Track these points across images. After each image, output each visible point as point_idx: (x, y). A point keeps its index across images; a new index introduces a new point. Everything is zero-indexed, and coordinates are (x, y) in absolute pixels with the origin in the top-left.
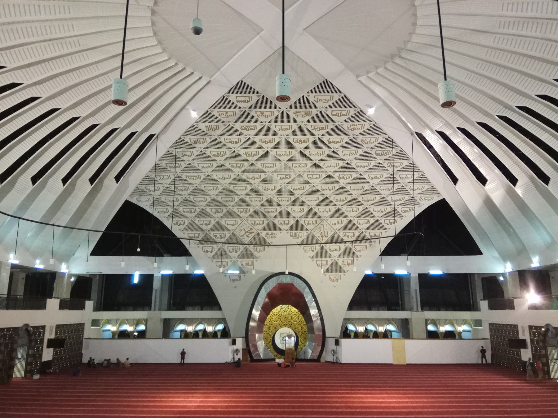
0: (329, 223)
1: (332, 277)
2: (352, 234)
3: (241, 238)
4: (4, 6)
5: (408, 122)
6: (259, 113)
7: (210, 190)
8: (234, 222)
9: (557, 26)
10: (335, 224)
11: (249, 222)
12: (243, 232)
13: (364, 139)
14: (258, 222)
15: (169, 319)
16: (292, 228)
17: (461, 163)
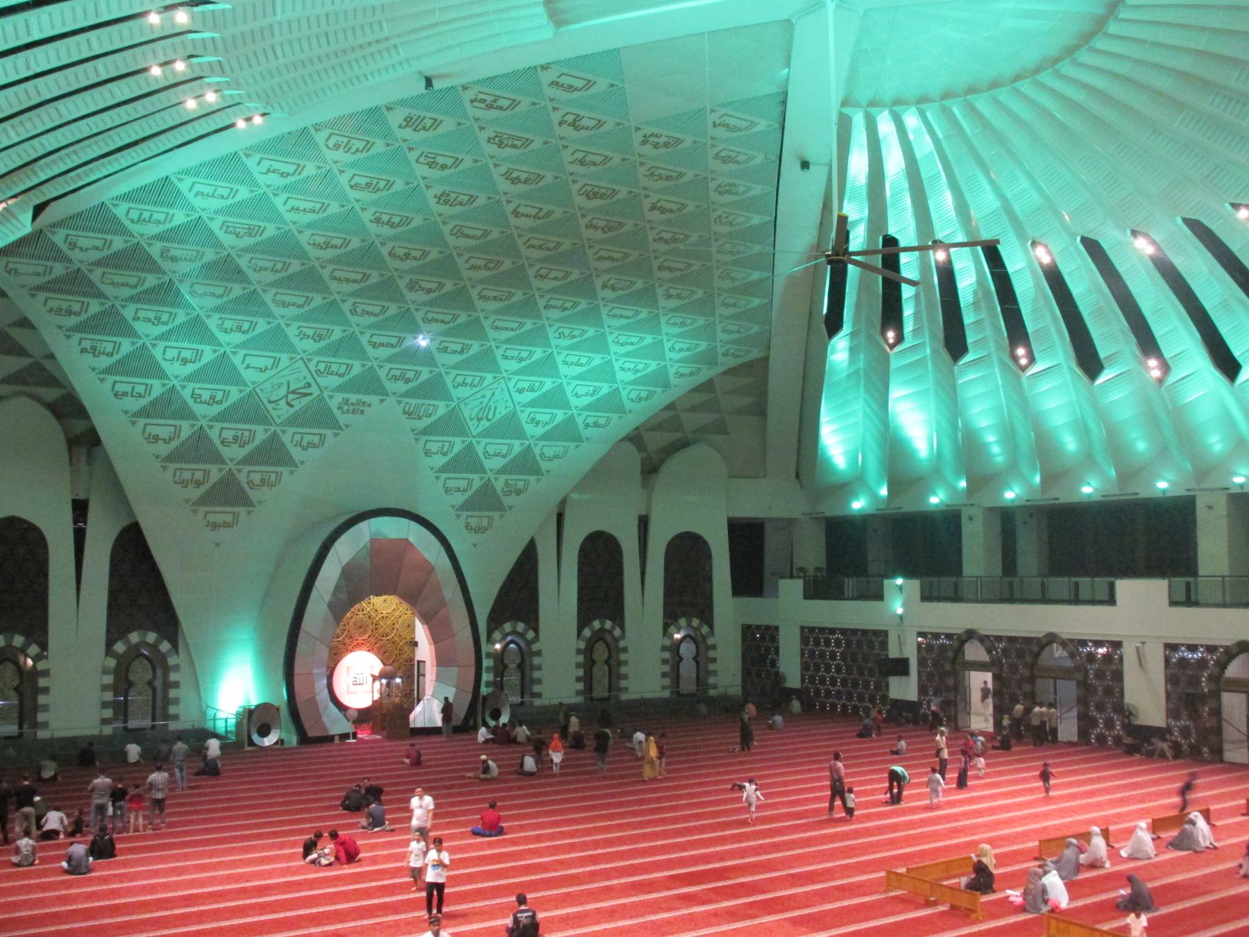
3: (270, 407)
5: (933, 286)
8: (269, 362)
11: (312, 366)
12: (283, 391)
15: (1002, 600)
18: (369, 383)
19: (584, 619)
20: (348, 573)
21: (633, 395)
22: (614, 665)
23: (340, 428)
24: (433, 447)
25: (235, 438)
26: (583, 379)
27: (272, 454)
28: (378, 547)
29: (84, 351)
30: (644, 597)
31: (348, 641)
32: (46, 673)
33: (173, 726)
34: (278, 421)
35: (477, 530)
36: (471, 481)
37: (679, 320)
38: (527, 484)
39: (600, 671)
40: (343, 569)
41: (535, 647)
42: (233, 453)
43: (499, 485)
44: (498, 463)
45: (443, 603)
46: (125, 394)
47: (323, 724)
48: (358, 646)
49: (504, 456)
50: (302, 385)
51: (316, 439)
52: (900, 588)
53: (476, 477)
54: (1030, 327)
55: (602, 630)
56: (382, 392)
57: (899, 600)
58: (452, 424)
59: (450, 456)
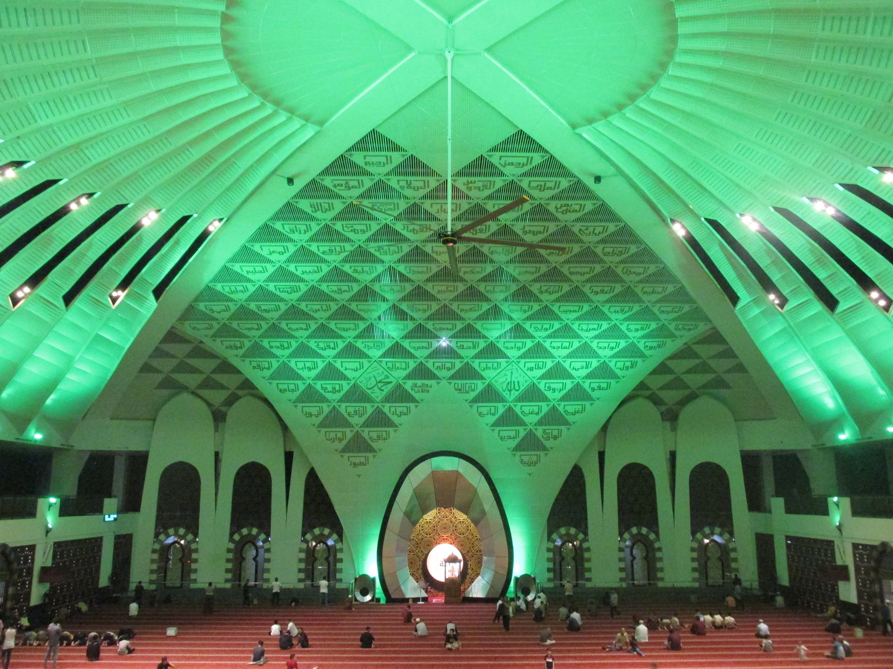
0: (522, 367)
1: (526, 459)
3: (369, 391)
6: (403, 184)
7: (317, 311)
10: (531, 369)
11: (383, 364)
13: (583, 228)
14: (398, 365)
16: (457, 376)
18: (422, 372)
21: (620, 365)
23: (417, 402)
24: (484, 410)
25: (355, 412)
26: (574, 360)
27: (380, 420)
28: (435, 475)
29: (254, 368)
30: (674, 513)
31: (436, 537)
34: (510, 400)
35: (529, 464)
36: (518, 432)
37: (618, 309)
38: (560, 431)
42: (356, 421)
43: (539, 432)
44: (535, 419)
45: (483, 513)
46: (285, 390)
47: (401, 591)
48: (445, 540)
49: (537, 414)
50: (383, 377)
51: (405, 410)
52: (837, 504)
53: (521, 429)
54: (870, 275)
56: (433, 376)
58: (490, 395)
59: (497, 416)
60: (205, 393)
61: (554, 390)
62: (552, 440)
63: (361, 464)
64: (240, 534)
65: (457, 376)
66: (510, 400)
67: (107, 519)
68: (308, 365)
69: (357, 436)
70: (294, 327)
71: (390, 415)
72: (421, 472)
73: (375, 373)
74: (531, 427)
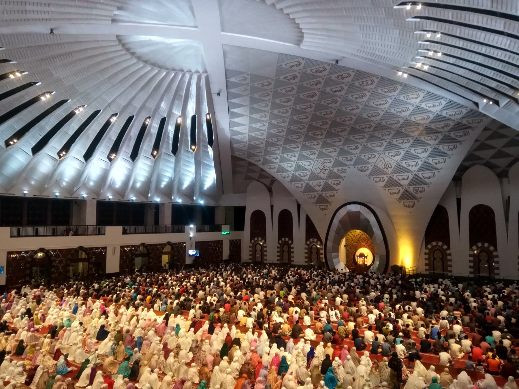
1: (407, 204)
2: (415, 163)
4: (360, 26)
9: (88, 2)
10: (393, 156)
11: (320, 161)
13: (361, 83)
14: (326, 161)
16: (356, 164)
17: (97, 119)
19: (280, 238)
20: (341, 222)
22: (290, 252)
24: (378, 180)
28: (350, 214)
32: (266, 247)
33: (497, 277)
35: (409, 207)
39: (286, 255)
40: (340, 221)
41: (292, 246)
42: (405, 183)
43: (411, 189)
49: (407, 179)
55: (285, 241)
57: (191, 231)
60: (263, 180)
61: (412, 166)
62: (419, 193)
63: (325, 209)
64: (282, 241)
65: (356, 164)
66: (389, 173)
67: (223, 233)
68: (289, 165)
69: (320, 196)
70: (274, 149)
71: (332, 185)
72: (342, 213)
73: (318, 166)
74: (405, 187)
